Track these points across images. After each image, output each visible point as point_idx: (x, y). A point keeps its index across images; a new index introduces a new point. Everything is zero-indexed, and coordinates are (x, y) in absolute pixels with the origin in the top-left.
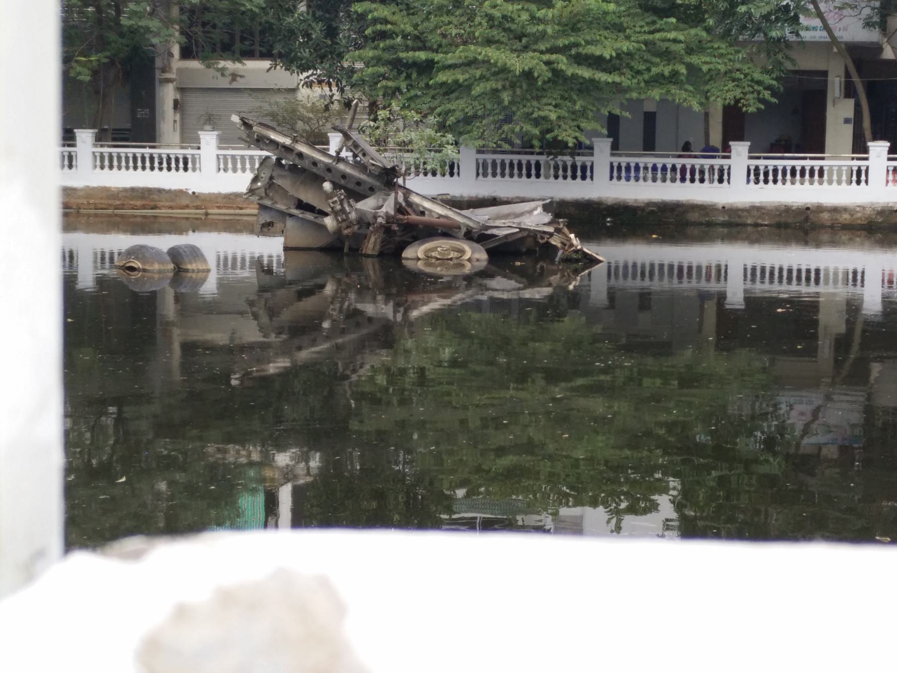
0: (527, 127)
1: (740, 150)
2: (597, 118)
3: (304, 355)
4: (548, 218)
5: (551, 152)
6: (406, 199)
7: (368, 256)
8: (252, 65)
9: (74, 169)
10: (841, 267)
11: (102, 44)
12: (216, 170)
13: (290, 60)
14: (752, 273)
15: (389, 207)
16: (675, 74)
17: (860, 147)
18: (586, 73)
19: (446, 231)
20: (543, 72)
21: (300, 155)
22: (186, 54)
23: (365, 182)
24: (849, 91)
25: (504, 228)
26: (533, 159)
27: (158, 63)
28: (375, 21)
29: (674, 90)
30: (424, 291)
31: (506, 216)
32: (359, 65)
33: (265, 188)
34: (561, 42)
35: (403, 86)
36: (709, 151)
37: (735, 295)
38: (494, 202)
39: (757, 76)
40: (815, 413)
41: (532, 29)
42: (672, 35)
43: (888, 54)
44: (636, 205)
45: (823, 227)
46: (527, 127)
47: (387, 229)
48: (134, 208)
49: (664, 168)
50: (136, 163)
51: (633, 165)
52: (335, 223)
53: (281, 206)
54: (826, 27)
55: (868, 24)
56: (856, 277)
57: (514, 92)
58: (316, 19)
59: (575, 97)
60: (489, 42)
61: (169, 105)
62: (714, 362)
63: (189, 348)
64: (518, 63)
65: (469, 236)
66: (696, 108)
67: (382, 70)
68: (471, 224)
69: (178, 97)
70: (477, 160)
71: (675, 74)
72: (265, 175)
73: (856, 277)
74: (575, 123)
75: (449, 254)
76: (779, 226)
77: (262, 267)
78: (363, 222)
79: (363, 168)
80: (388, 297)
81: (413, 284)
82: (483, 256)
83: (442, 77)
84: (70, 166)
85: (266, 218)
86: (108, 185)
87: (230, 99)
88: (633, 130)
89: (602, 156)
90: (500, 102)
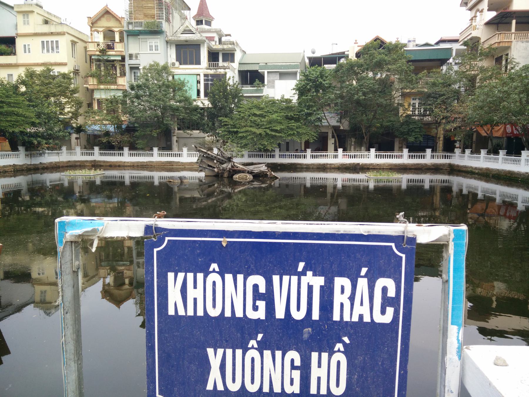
0: (260, 146)
1: (309, 151)
2: (276, 144)
3: (210, 201)
4: (266, 168)
5: (266, 152)
8: (194, 131)
11: (159, 127)
12: (187, 157)
13: (204, 131)
15: (230, 166)
16: (294, 133)
17: (336, 150)
18: (274, 133)
19: (243, 171)
20: (263, 133)
21: (209, 154)
22: (179, 129)
24: (333, 137)
26: (261, 153)
27: (172, 131)
28: (224, 122)
29: (294, 137)
30: (238, 185)
31: (256, 168)
32: (220, 132)
33: (200, 162)
34: (267, 126)
36: (302, 151)
37: (308, 185)
39: (313, 134)
41: (261, 123)
43: (342, 128)
46: (260, 146)
47: (229, 171)
50: (168, 155)
54: (328, 122)
55: (337, 122)
56: (336, 180)
58: (210, 121)
60: (251, 126)
62: (304, 200)
63: (181, 199)
64: (258, 131)
65: (248, 172)
66: (299, 141)
67: (226, 133)
71: (294, 133)
72: (200, 159)
73: (336, 180)
76: (318, 168)
78: (224, 170)
79: (224, 157)
81: (235, 184)
82: (252, 177)
83: (240, 135)
84: (360, 315)
85: (201, 169)
87: (189, 140)
88: (284, 147)
89: (277, 153)
90: (254, 140)
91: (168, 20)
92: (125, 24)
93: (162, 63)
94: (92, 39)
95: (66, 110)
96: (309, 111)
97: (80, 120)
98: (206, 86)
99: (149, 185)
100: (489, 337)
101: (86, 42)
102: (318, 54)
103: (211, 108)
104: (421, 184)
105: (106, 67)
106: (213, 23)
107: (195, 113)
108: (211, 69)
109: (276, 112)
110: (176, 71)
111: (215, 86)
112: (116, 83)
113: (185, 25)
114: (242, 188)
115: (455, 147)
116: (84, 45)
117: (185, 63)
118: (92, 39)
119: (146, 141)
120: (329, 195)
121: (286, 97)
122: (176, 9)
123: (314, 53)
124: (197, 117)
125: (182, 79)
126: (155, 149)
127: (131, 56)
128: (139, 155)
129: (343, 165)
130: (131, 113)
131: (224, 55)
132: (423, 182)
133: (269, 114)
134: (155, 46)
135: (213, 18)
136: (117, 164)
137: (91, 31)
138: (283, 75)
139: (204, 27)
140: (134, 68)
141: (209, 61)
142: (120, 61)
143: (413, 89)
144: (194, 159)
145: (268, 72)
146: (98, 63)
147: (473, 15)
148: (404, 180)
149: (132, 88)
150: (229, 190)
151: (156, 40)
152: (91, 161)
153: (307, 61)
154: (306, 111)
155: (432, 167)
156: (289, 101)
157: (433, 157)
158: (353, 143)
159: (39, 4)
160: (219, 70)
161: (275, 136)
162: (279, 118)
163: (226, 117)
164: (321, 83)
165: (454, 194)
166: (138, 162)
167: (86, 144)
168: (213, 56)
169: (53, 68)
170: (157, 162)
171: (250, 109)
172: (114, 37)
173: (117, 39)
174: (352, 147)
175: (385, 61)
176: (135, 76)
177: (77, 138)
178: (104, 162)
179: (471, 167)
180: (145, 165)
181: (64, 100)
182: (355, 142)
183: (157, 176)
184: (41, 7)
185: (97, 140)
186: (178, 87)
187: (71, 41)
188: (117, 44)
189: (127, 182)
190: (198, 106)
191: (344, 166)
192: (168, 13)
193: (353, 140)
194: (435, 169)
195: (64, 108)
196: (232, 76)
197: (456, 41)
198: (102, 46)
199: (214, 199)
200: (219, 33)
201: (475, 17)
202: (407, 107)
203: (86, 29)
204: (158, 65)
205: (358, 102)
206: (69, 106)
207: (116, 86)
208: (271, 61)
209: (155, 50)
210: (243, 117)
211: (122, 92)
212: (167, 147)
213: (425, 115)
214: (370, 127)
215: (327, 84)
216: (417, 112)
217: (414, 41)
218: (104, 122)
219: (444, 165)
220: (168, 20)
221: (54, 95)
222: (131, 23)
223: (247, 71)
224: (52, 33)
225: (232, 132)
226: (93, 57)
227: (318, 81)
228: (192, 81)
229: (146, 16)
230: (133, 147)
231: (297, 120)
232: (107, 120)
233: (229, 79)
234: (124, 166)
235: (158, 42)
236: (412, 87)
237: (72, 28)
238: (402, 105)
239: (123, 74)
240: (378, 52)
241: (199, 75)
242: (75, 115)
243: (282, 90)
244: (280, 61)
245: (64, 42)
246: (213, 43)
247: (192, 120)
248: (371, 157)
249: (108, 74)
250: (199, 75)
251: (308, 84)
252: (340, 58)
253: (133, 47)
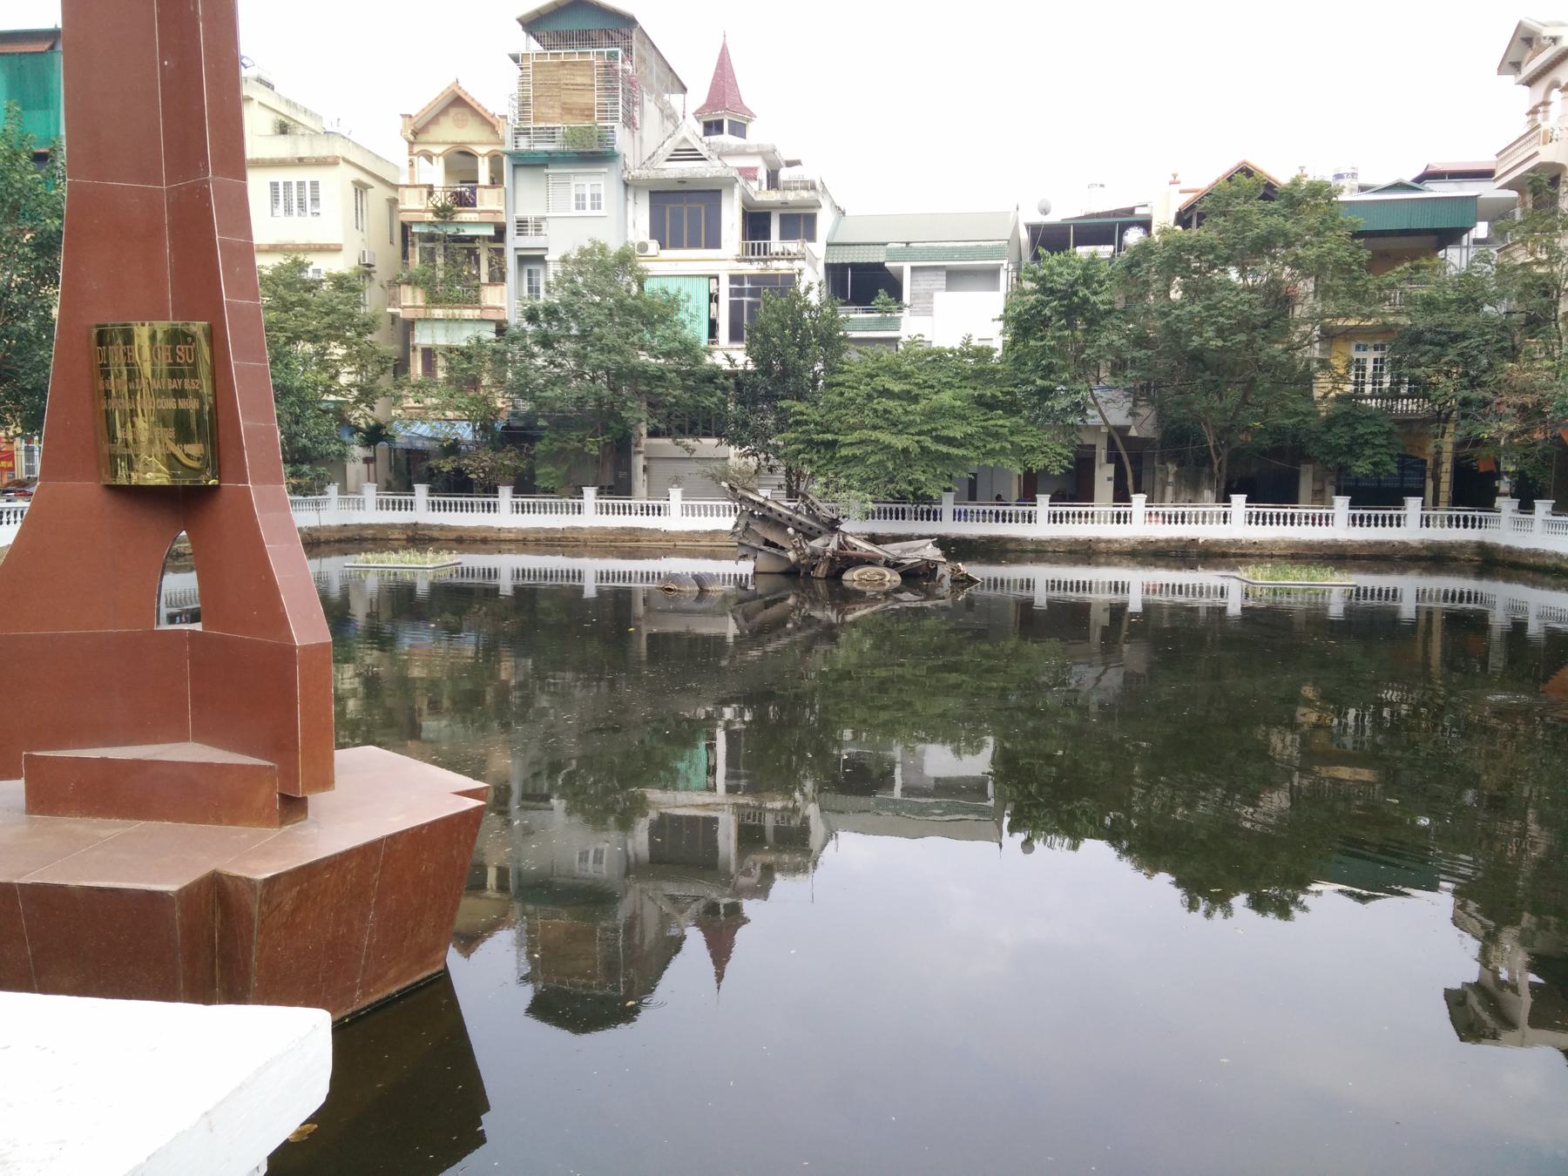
0: (904, 486)
5: (922, 504)
10: (1081, 579)
11: (606, 429)
14: (1053, 585)
15: (833, 545)
16: (1003, 449)
18: (944, 449)
19: (871, 561)
21: (770, 509)
22: (653, 434)
25: (911, 559)
28: (795, 414)
34: (926, 428)
35: (815, 458)
38: (909, 538)
39: (1059, 450)
40: (1098, 679)
41: (904, 419)
42: (1000, 422)
43: (1133, 433)
45: (1101, 553)
46: (904, 486)
47: (832, 560)
60: (875, 428)
61: (641, 469)
64: (900, 442)
65: (887, 564)
71: (1003, 449)
72: (742, 523)
76: (1070, 552)
77: (740, 582)
78: (815, 555)
79: (816, 519)
80: (833, 606)
82: (899, 578)
85: (743, 551)
89: (948, 505)
90: (886, 468)
91: (630, 122)
92: (506, 132)
93: (614, 247)
94: (412, 175)
95: (344, 380)
96: (1047, 383)
97: (380, 411)
98: (735, 308)
99: (568, 595)
101: (395, 187)
102: (1054, 218)
103: (754, 374)
105: (450, 257)
106: (751, 129)
107: (710, 388)
108: (751, 261)
109: (949, 385)
110: (654, 268)
111: (762, 309)
112: (478, 301)
113: (679, 136)
114: (1499, 697)
115: (1497, 492)
116: (391, 194)
117: (677, 244)
118: (412, 175)
119: (565, 468)
120: (1096, 635)
121: (975, 343)
122: (651, 91)
123: (1045, 212)
124: (715, 399)
125: (672, 291)
126: (590, 493)
127: (522, 225)
128: (545, 509)
129: (1145, 543)
130: (523, 389)
131: (783, 218)
132: (1394, 596)
133: (927, 391)
134: (593, 197)
135: (752, 115)
136: (479, 536)
137: (411, 153)
138: (956, 278)
139: (726, 139)
140: (531, 260)
141: (744, 238)
142: (490, 238)
143: (1369, 317)
144: (727, 523)
145: (913, 269)
146: (429, 245)
147: (1539, 99)
148: (1335, 589)
149: (531, 317)
150: (832, 616)
151: (595, 180)
152: (406, 527)
153: (1024, 236)
154: (1039, 382)
155: (1425, 553)
156: (983, 354)
157: (1426, 522)
158: (1171, 479)
159: (265, 76)
160: (775, 264)
161: (948, 456)
162: (959, 403)
163: (798, 399)
164: (1086, 300)
165: (1496, 633)
166: (537, 530)
167: (390, 477)
168: (756, 223)
169: (308, 258)
170: (593, 530)
171: (871, 376)
172: (476, 171)
173: (484, 176)
174: (1170, 490)
175: (1285, 235)
176: (530, 281)
177: (367, 460)
178: (442, 528)
179: (1556, 554)
181: (337, 351)
182: (1176, 475)
183: (592, 571)
184: (270, 86)
185: (423, 467)
186: (653, 314)
187: (354, 183)
188: (486, 191)
189: (506, 585)
190: (718, 367)
191: (1152, 548)
192: (630, 102)
193: (1172, 468)
194: (1435, 559)
195: (337, 373)
196: (811, 280)
197: (1486, 175)
198: (440, 198)
199: (785, 641)
200: (771, 157)
201: (1546, 103)
202: (1342, 371)
203: (393, 150)
204: (603, 249)
205: (1197, 358)
206: (352, 369)
207: (478, 312)
208: (922, 236)
209: (593, 207)
210: (852, 400)
211: (493, 328)
212: (618, 488)
213: (1395, 395)
214: (1229, 430)
215: (1103, 303)
216: (1368, 389)
217: (1354, 175)
218: (450, 414)
219: (1462, 546)
220: (630, 122)
221: (314, 338)
222: (526, 132)
223: (844, 266)
224: (301, 159)
225: (818, 444)
226: (415, 229)
227: (1075, 293)
228: (700, 292)
229: (567, 110)
230: (524, 486)
231: (1012, 408)
232: (458, 408)
233: (809, 289)
235: (600, 183)
236: (1366, 310)
237: (357, 146)
238: (1325, 365)
239: (498, 277)
240: (1246, 212)
241: (717, 277)
242: (367, 394)
243: (960, 321)
244: (948, 237)
245: (335, 185)
246: (755, 185)
247: (696, 407)
248: (1236, 521)
249: (454, 277)
250: (717, 277)
251: (1044, 304)
252: (1124, 227)
253: (530, 198)
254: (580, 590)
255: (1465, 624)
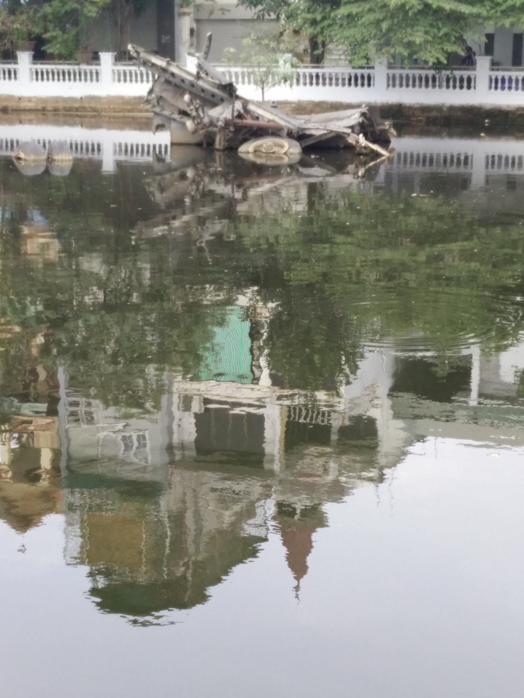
6: (245, 108)
7: (218, 150)
9: (99, 82)
19: (274, 131)
21: (173, 75)
23: (217, 95)
44: (508, 109)
48: (140, 111)
49: (462, 80)
51: (507, 78)
52: (193, 125)
53: (167, 113)
57: (393, 21)
59: (441, 25)
65: (290, 135)
68: (291, 127)
69: (195, 26)
70: (388, 75)
74: (440, 46)
75: (272, 149)
86: (13, 531)
88: (504, 48)
100: (132, 618)
104: (462, 169)
166: (56, 99)
180: (77, 109)
234: (18, 111)
254: (99, 164)
255: (448, 182)
